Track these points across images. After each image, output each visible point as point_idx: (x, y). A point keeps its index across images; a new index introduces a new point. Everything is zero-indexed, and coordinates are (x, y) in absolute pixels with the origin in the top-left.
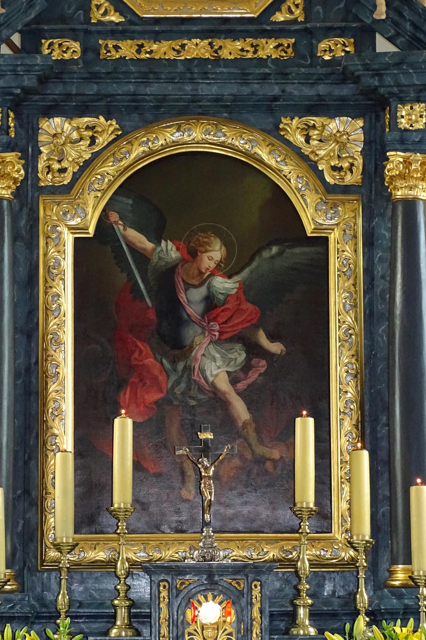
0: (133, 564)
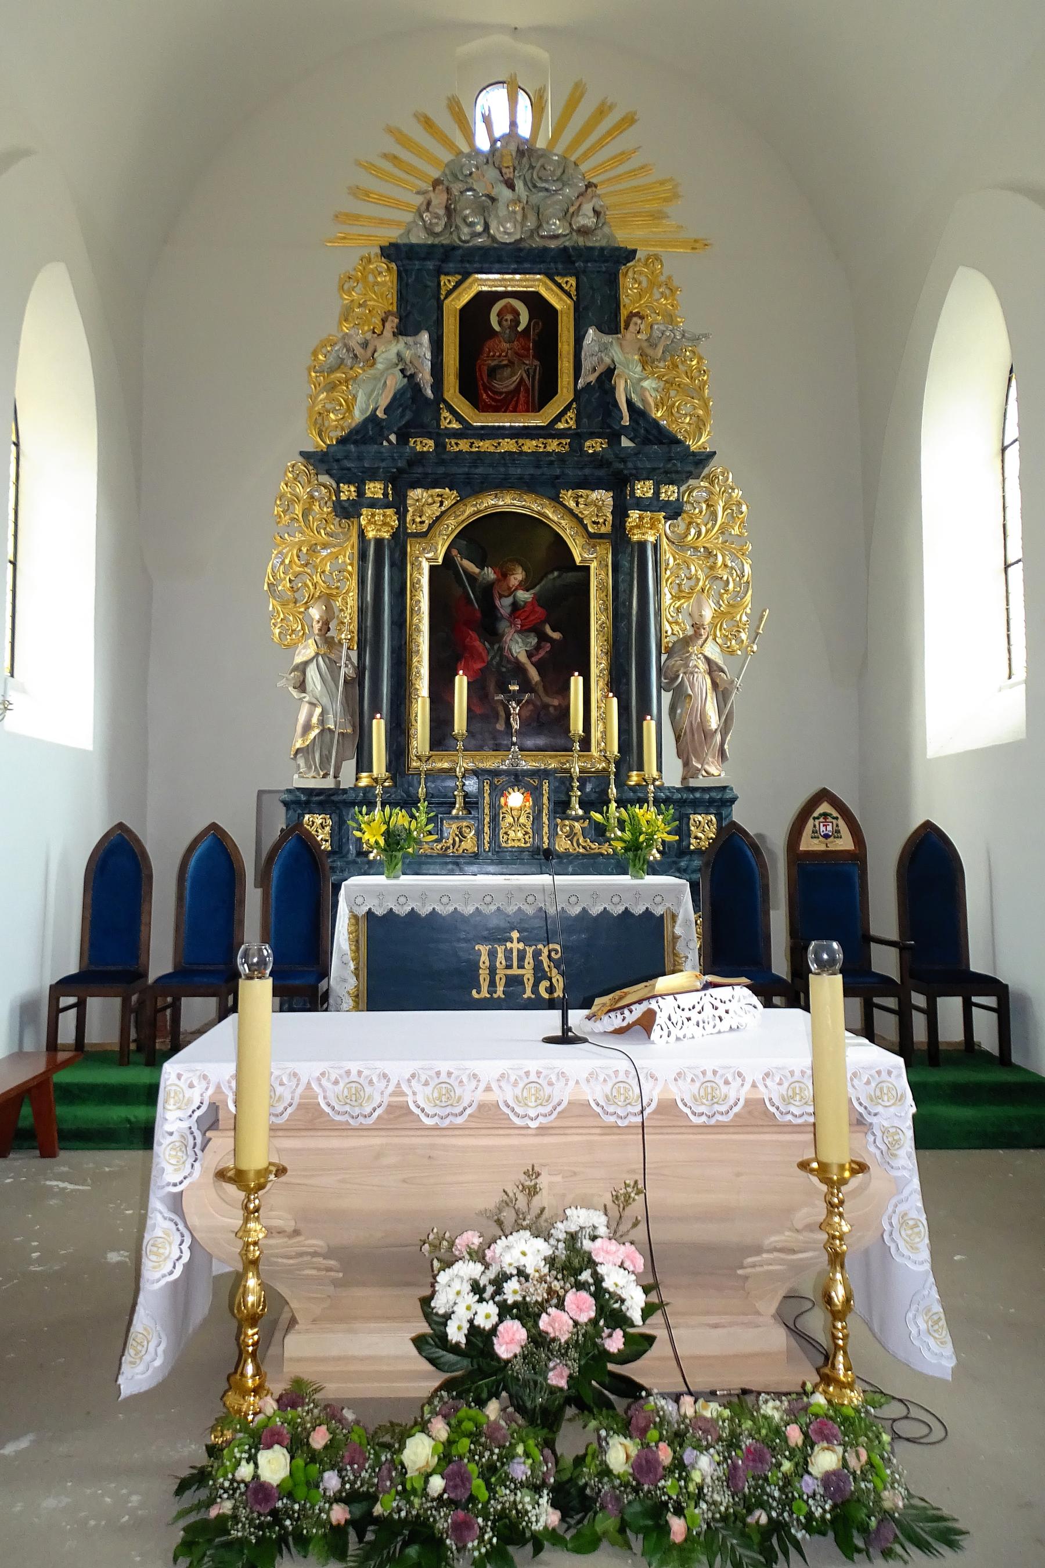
0: (466, 770)
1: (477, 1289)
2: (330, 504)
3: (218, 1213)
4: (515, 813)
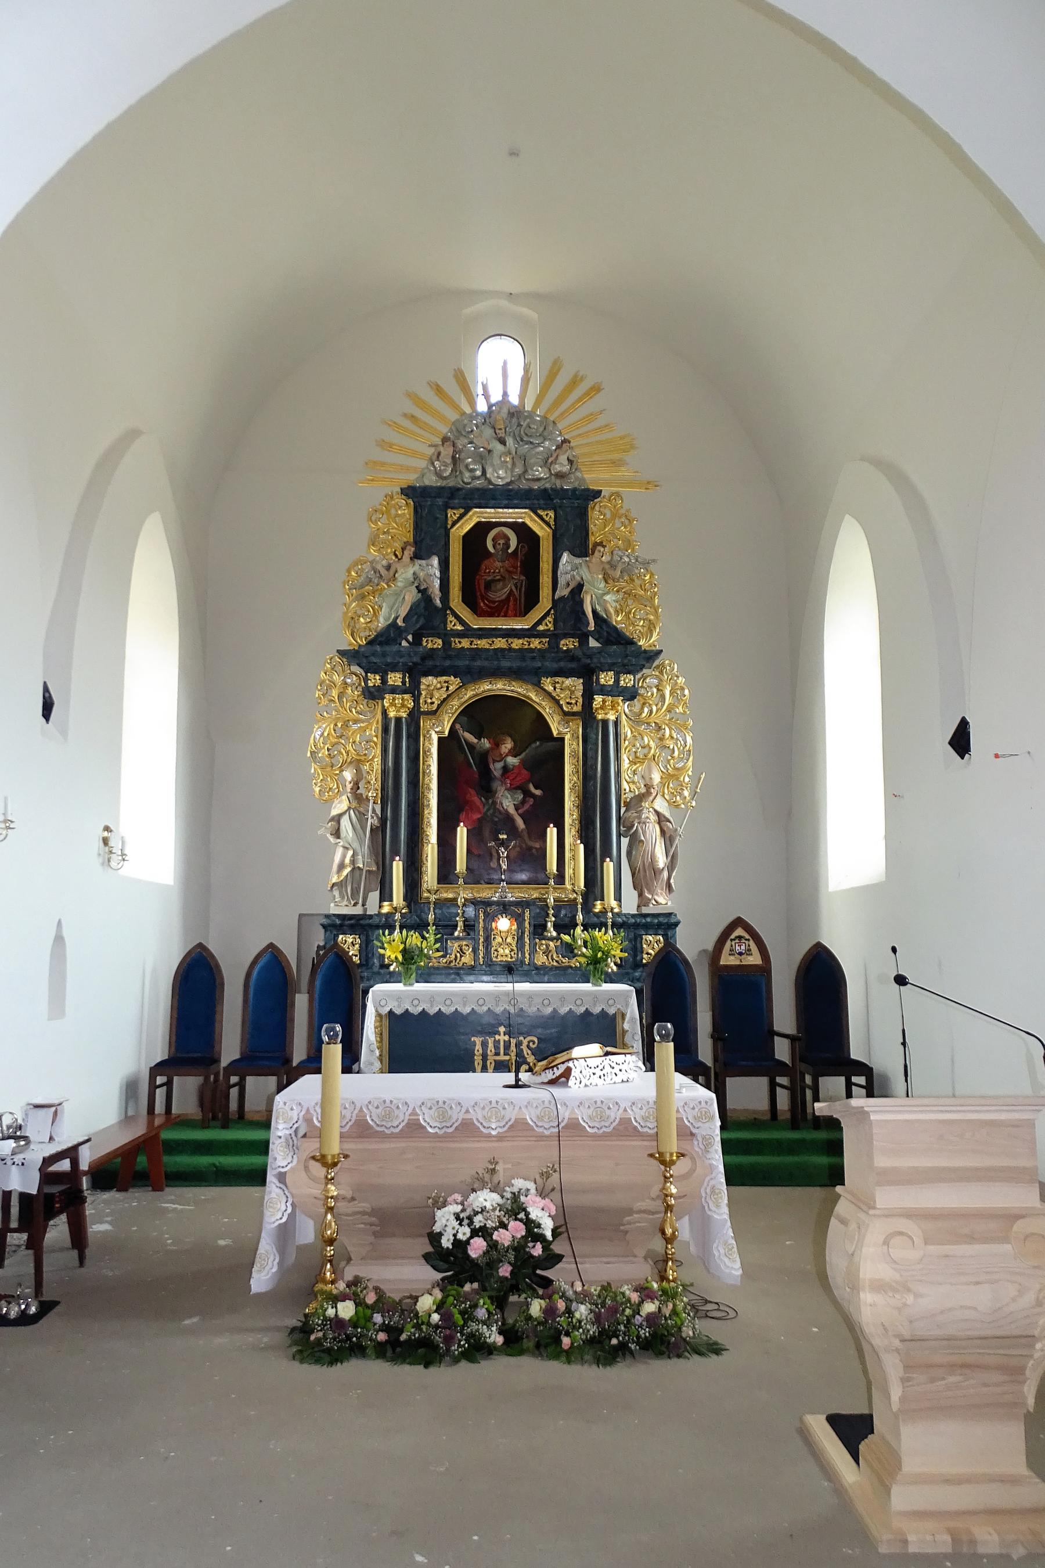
0: (466, 900)
1: (457, 1217)
2: (360, 689)
3: (309, 1185)
4: (503, 935)
